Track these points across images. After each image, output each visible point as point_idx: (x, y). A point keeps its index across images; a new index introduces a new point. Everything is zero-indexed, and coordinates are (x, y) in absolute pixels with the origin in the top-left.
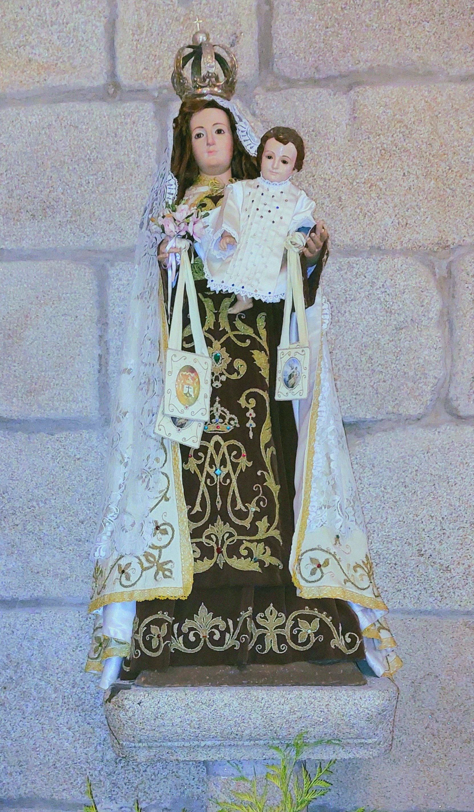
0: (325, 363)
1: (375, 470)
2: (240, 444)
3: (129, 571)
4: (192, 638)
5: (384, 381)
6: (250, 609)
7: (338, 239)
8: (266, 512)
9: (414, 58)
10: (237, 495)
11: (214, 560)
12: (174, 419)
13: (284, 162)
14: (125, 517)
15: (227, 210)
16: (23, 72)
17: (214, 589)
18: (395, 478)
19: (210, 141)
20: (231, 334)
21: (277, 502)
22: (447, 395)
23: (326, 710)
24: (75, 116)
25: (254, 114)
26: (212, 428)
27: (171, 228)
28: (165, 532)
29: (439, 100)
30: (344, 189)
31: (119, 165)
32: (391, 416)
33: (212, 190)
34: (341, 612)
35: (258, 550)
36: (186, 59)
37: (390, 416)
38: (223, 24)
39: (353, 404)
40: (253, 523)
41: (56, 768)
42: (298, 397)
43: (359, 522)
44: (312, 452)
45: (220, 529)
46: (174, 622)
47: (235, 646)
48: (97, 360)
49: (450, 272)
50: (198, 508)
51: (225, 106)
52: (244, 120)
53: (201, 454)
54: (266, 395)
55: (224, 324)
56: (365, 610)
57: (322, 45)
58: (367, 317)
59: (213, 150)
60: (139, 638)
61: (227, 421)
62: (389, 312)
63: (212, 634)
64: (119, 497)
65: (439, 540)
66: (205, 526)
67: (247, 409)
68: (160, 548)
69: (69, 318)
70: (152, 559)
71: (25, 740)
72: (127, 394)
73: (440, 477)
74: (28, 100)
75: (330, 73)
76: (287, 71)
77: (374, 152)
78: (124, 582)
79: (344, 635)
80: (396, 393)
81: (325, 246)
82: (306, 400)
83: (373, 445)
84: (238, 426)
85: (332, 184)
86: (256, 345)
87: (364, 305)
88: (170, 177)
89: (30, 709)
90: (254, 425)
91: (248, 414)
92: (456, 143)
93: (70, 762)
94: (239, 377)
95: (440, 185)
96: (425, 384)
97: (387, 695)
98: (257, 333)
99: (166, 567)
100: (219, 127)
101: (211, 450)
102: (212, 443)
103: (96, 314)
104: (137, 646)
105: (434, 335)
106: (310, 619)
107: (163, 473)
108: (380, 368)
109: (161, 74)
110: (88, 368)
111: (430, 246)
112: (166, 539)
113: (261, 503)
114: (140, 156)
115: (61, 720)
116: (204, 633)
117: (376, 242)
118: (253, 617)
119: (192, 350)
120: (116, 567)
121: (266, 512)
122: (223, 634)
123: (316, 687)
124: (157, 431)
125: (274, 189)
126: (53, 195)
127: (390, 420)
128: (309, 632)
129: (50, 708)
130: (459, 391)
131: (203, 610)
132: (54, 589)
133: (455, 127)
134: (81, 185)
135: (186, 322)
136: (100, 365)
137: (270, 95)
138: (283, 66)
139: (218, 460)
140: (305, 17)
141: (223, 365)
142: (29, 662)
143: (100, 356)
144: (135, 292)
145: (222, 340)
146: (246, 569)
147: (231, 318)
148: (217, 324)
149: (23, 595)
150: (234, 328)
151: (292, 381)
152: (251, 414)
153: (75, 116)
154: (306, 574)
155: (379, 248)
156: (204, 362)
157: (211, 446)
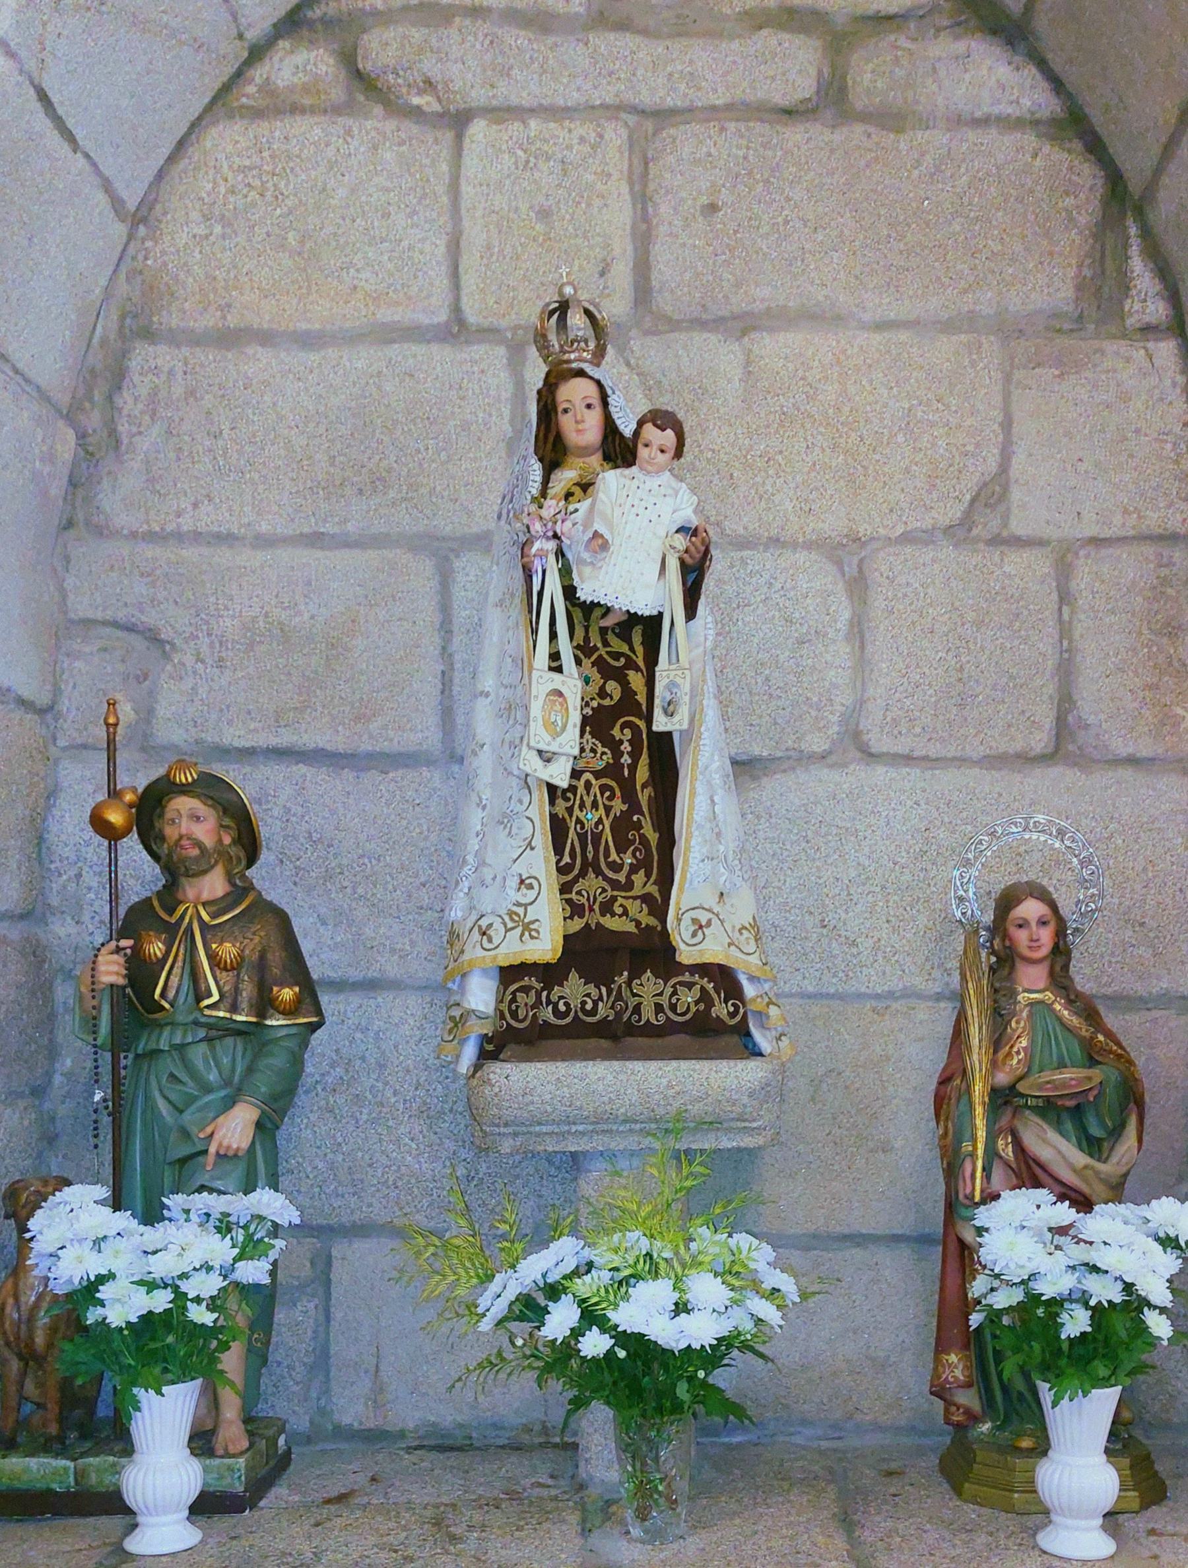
0: (710, 686)
1: (773, 820)
2: (613, 784)
3: (491, 932)
4: (562, 1008)
6: (626, 973)
8: (643, 864)
9: (821, 298)
10: (611, 844)
11: (585, 920)
12: (540, 752)
13: (662, 451)
14: (485, 870)
16: (346, 302)
17: (587, 952)
19: (579, 418)
20: (603, 651)
21: (655, 853)
22: (857, 725)
24: (411, 361)
25: (628, 364)
26: (581, 765)
27: (537, 527)
28: (531, 887)
29: (849, 352)
31: (465, 426)
32: (791, 753)
34: (723, 978)
35: (634, 907)
36: (552, 313)
37: (790, 753)
39: (747, 737)
40: (628, 877)
42: (677, 727)
43: (746, 877)
44: (693, 794)
45: (591, 884)
46: (543, 989)
48: (439, 677)
49: (860, 570)
50: (567, 859)
51: (596, 376)
52: (617, 393)
53: (569, 795)
54: (642, 724)
55: (595, 640)
56: (752, 979)
58: (763, 627)
59: (581, 428)
60: (504, 1007)
62: (789, 621)
63: (584, 1003)
64: (477, 847)
66: (575, 880)
67: (621, 742)
68: (526, 906)
70: (516, 918)
71: (360, 1154)
72: (484, 723)
73: (847, 829)
74: (353, 338)
75: (720, 313)
76: (668, 309)
77: (772, 417)
78: (486, 945)
79: (726, 1002)
80: (798, 724)
81: (707, 551)
82: (687, 731)
83: (779, 791)
84: (611, 761)
85: (722, 456)
86: (631, 665)
87: (759, 612)
88: (533, 461)
89: (365, 1117)
90: (629, 761)
91: (622, 748)
92: (868, 408)
93: (413, 1181)
95: (850, 460)
96: (831, 713)
97: (770, 1067)
98: (632, 649)
99: (532, 927)
100: (589, 401)
101: (581, 790)
103: (437, 619)
104: (502, 1017)
105: (840, 652)
106: (690, 986)
107: (528, 818)
109: (516, 308)
110: (427, 688)
112: (531, 895)
114: (490, 415)
115: (402, 1129)
116: (575, 1004)
117: (774, 532)
118: (629, 983)
119: (559, 670)
120: (476, 928)
121: (643, 864)
122: (595, 1003)
124: (521, 766)
125: (653, 482)
126: (384, 463)
127: (789, 758)
128: (689, 1000)
131: (573, 976)
132: (392, 969)
135: (553, 635)
136: (443, 684)
137: (649, 340)
138: (664, 302)
139: (589, 801)
140: (691, 241)
141: (593, 689)
142: (363, 1058)
143: (443, 672)
144: (493, 598)
146: (621, 929)
147: (603, 631)
148: (587, 639)
149: (355, 974)
150: (606, 644)
151: (671, 708)
152: (626, 747)
154: (686, 935)
155: (778, 540)
156: (572, 684)
157: (581, 784)
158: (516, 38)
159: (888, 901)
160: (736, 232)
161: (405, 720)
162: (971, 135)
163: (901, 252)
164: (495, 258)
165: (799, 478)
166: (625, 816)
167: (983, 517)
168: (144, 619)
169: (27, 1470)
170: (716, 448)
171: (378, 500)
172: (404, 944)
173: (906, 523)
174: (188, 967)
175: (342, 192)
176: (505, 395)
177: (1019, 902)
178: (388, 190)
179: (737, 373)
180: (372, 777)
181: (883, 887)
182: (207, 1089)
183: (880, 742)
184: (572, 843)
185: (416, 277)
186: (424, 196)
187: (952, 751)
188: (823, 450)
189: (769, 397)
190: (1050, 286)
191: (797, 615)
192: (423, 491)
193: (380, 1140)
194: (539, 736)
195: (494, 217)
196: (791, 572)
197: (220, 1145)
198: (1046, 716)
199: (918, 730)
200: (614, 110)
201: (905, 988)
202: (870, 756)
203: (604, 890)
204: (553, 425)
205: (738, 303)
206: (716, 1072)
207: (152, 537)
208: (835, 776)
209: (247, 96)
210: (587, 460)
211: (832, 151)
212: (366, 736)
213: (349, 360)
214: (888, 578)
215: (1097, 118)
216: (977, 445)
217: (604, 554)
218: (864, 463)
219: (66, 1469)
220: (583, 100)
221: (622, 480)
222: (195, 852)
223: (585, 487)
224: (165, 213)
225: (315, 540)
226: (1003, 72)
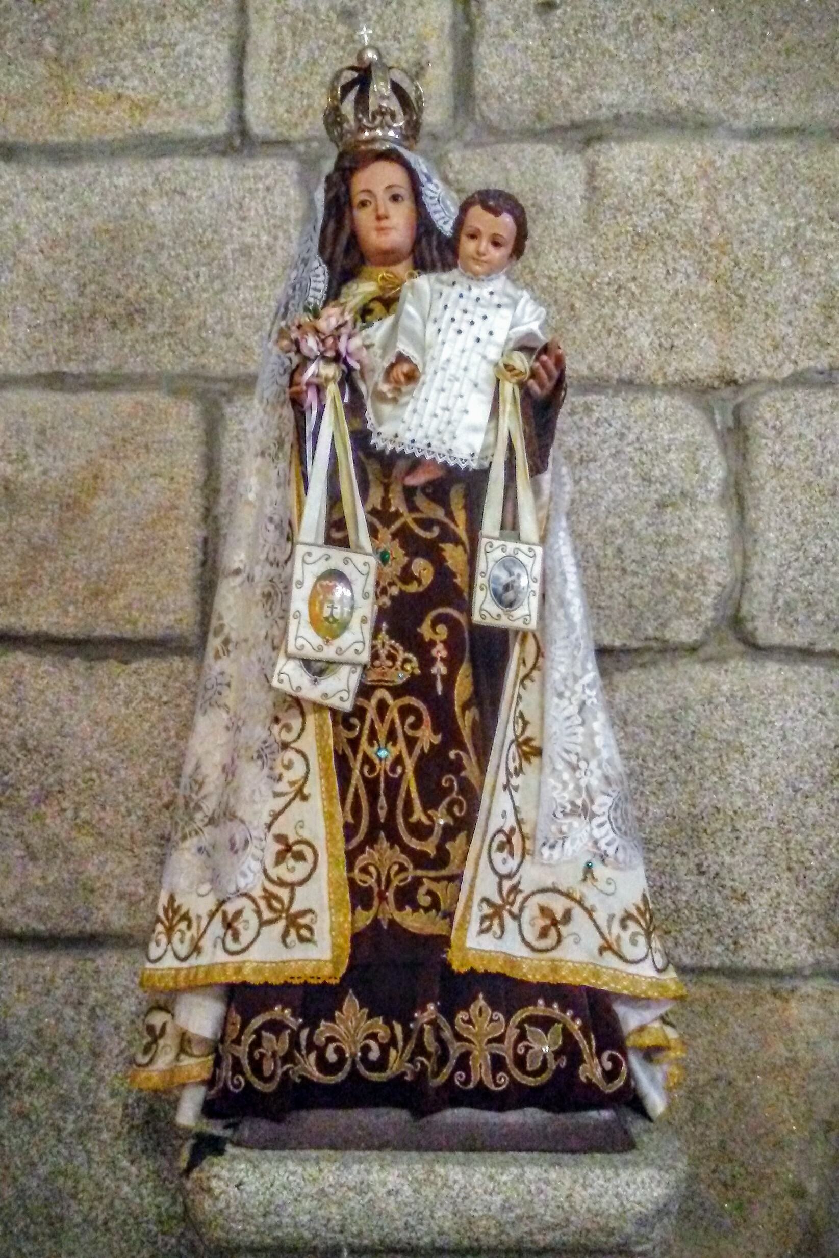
1: (630, 729)
4: (331, 1056)
5: (641, 588)
7: (575, 367)
10: (414, 794)
11: (371, 914)
15: (404, 321)
18: (659, 743)
19: (381, 211)
20: (408, 518)
23: (566, 1205)
26: (373, 677)
30: (578, 293)
31: (245, 251)
32: (654, 644)
33: (382, 288)
36: (346, 89)
38: (400, 50)
40: (440, 848)
41: (108, 1230)
45: (383, 856)
46: (301, 1027)
47: (404, 1074)
49: (738, 420)
57: (546, 83)
58: (614, 487)
61: (399, 663)
62: (647, 479)
65: (729, 848)
67: (433, 643)
68: (292, 886)
69: (160, 480)
76: (494, 117)
77: (623, 238)
79: (599, 1054)
80: (660, 607)
84: (418, 672)
88: (316, 264)
89: (70, 1127)
92: (744, 227)
94: (421, 589)
95: (722, 288)
98: (450, 514)
100: (396, 191)
102: (374, 702)
103: (199, 476)
106: (545, 1023)
108: (633, 567)
110: (184, 562)
111: (708, 381)
112: (302, 869)
113: (456, 810)
114: (276, 238)
117: (626, 373)
119: (344, 543)
122: (385, 1050)
123: (548, 1155)
129: (102, 1125)
130: (755, 605)
133: (743, 203)
134: (187, 279)
136: (205, 553)
137: (468, 153)
139: (382, 731)
141: (393, 569)
142: (72, 1043)
145: (394, 527)
147: (409, 493)
148: (386, 501)
149: (70, 926)
150: (413, 508)
151: (510, 595)
152: (440, 651)
155: (631, 382)
157: (371, 706)
159: (788, 842)
160: (576, 32)
161: (154, 598)
163: (779, 53)
164: (286, 63)
165: (657, 309)
166: (439, 751)
170: (553, 274)
172: (137, 885)
173: (796, 363)
176: (294, 215)
179: (579, 190)
181: (781, 822)
183: (770, 631)
184: (356, 795)
185: (192, 84)
188: (688, 277)
189: (619, 215)
191: (657, 472)
192: (190, 324)
195: (288, 19)
196: (649, 420)
199: (820, 617)
201: (818, 963)
202: (755, 649)
203: (403, 868)
204: (347, 222)
205: (581, 110)
206: (584, 1186)
208: (711, 674)
210: (393, 269)
213: (109, 177)
214: (774, 427)
217: (410, 387)
218: (741, 291)
221: (438, 286)
223: (388, 302)
225: (55, 381)
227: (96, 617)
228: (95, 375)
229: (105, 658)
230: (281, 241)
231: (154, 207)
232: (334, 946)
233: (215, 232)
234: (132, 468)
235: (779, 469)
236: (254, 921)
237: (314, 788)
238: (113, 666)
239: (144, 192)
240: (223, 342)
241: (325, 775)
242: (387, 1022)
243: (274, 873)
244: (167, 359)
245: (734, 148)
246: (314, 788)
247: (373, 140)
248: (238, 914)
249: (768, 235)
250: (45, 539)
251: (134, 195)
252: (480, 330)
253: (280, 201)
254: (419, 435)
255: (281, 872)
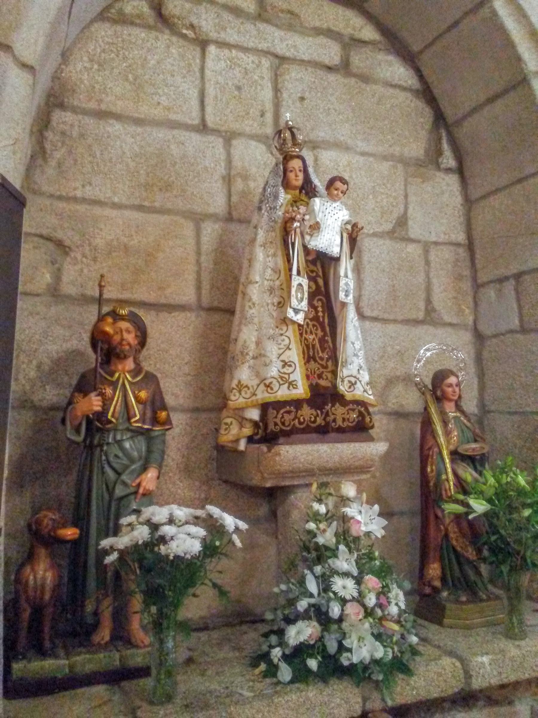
3: (272, 386)
4: (302, 420)
67: (318, 307)
68: (289, 374)
86: (318, 276)
106: (353, 410)
112: (290, 370)
122: (315, 418)
139: (309, 330)
152: (320, 309)
153: (183, 138)
158: (226, 16)
162: (391, 90)
167: (399, 230)
168: (56, 235)
169: (42, 668)
171: (168, 195)
174: (123, 403)
175: (153, 62)
177: (448, 377)
178: (173, 65)
180: (164, 315)
182: (132, 461)
186: (189, 71)
187: (392, 317)
190: (416, 148)
193: (166, 483)
194: (294, 302)
195: (218, 86)
197: (145, 489)
198: (422, 305)
199: (380, 308)
200: (267, 53)
207: (60, 198)
209: (111, 13)
211: (345, 86)
212: (163, 297)
215: (436, 92)
216: (397, 203)
219: (64, 665)
220: (255, 47)
222: (127, 347)
224: (71, 55)
225: (140, 208)
226: (402, 70)
227: (161, 296)
228: (155, 207)
229: (163, 311)
230: (218, 167)
231: (172, 147)
232: (304, 389)
233: (195, 160)
234: (171, 243)
235: (370, 262)
236: (278, 385)
237: (293, 346)
238: (166, 314)
239: (169, 141)
240: (200, 200)
241: (296, 342)
242: (316, 411)
243: (282, 371)
244: (180, 204)
245: (357, 157)
246: (293, 346)
247: (292, 152)
248: (271, 383)
249: (366, 188)
250: (140, 266)
251: (165, 141)
252: (336, 216)
253: (217, 152)
254: (323, 246)
255: (285, 370)
